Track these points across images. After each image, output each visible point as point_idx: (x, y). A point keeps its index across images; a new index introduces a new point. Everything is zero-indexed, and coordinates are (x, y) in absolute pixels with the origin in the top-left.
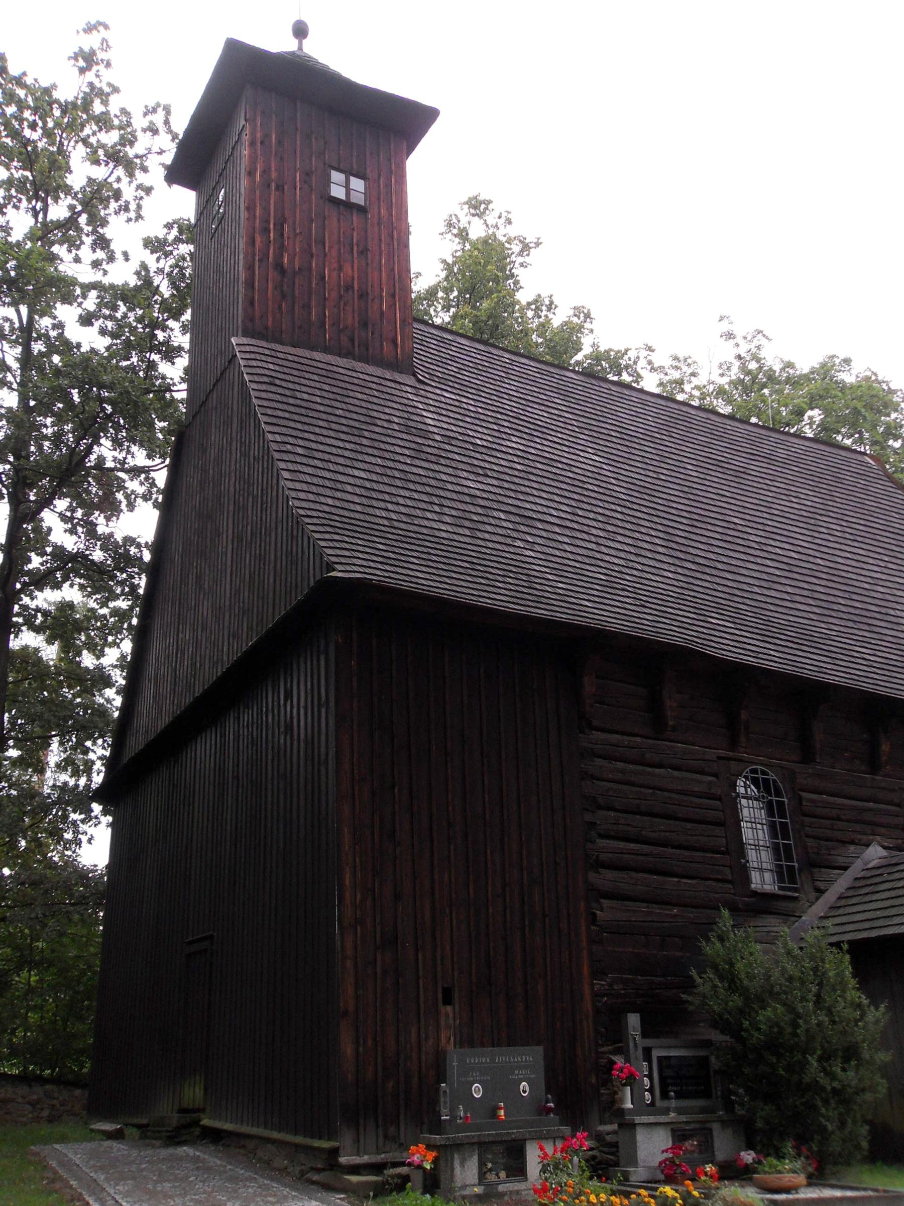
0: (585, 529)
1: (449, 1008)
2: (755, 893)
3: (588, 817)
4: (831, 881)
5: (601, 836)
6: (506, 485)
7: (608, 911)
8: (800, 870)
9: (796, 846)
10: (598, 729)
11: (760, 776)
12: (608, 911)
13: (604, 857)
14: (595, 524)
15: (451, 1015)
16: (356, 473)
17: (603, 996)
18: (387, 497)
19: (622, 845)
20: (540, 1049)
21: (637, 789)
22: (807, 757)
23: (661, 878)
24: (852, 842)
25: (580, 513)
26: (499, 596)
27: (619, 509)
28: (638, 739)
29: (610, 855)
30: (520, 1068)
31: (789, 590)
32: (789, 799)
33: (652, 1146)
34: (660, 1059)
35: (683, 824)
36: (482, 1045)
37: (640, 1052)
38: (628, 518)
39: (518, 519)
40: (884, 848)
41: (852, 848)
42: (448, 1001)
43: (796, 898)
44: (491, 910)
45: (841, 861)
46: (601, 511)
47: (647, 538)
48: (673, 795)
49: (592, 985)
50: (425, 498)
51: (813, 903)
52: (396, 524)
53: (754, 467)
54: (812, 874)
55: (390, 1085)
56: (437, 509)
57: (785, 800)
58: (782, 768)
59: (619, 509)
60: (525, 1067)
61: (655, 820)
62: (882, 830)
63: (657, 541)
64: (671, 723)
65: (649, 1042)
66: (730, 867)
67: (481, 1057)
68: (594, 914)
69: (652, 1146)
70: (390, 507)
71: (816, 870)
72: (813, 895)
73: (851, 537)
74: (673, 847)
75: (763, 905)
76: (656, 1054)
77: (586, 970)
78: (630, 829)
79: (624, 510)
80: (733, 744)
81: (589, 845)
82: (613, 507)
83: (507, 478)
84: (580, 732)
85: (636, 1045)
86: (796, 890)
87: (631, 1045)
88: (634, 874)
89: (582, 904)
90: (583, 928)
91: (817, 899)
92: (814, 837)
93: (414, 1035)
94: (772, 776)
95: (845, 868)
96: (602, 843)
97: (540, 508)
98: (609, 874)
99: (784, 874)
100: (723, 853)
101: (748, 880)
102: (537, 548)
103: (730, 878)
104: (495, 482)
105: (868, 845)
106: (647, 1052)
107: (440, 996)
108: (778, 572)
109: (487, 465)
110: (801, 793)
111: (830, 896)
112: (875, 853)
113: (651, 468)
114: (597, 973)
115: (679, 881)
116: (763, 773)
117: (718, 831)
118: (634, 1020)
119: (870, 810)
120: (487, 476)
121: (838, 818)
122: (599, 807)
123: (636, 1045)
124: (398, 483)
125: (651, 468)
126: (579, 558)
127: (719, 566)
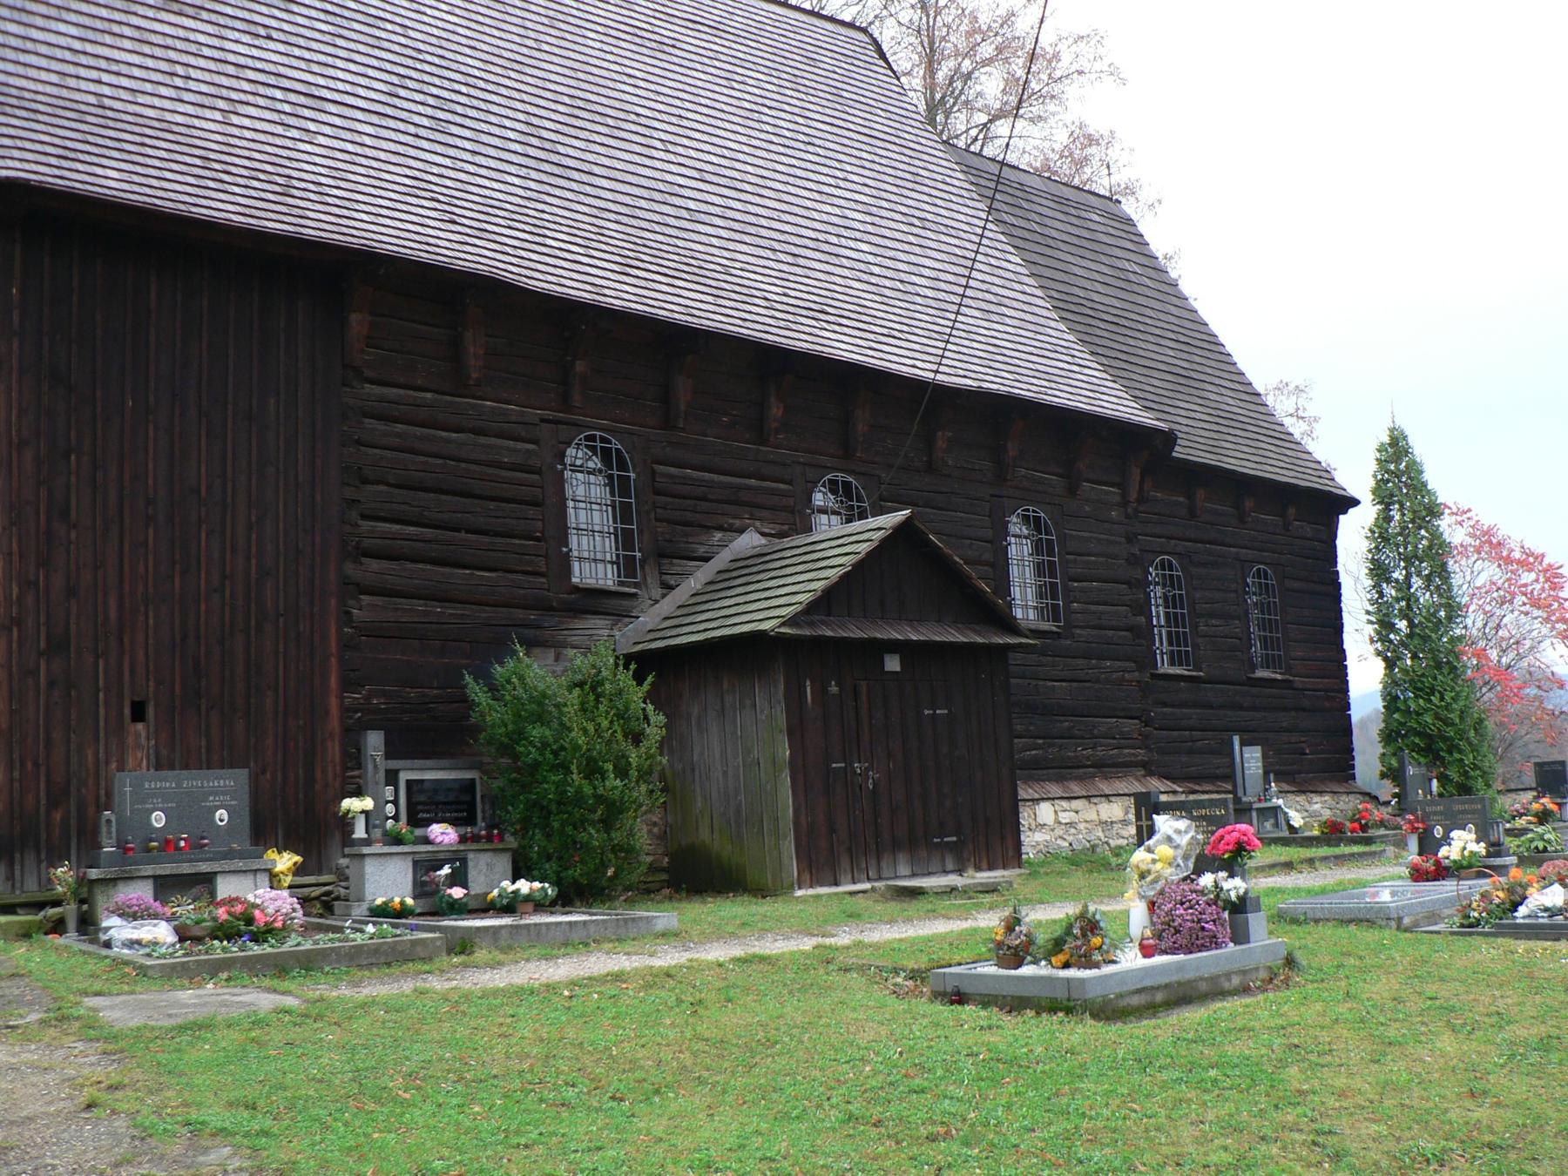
0: (404, 115)
1: (140, 726)
2: (576, 589)
3: (349, 493)
4: (686, 575)
5: (364, 517)
6: (297, 52)
7: (365, 610)
8: (643, 561)
9: (640, 532)
10: (372, 382)
11: (599, 444)
12: (365, 610)
13: (367, 543)
14: (421, 109)
15: (144, 735)
16: (62, 27)
17: (356, 711)
18: (103, 64)
19: (396, 527)
20: (242, 774)
21: (422, 459)
22: (667, 423)
23: (447, 570)
24: (720, 528)
25: (402, 92)
26: (226, 205)
27: (464, 89)
28: (429, 395)
29: (379, 541)
30: (216, 794)
31: (692, 204)
32: (638, 474)
33: (388, 880)
34: (408, 782)
35: (481, 502)
36: (172, 767)
37: (381, 775)
38: (476, 103)
39: (302, 100)
40: (763, 534)
41: (718, 535)
42: (138, 714)
43: (635, 595)
44: (203, 607)
45: (701, 550)
46: (435, 91)
47: (497, 131)
48: (473, 467)
49: (342, 698)
50: (164, 66)
51: (657, 602)
52: (107, 102)
53: (690, 40)
54: (660, 565)
55: (58, 816)
56: (179, 82)
57: (632, 475)
58: (632, 433)
59: (464, 89)
60: (224, 793)
61: (444, 497)
62: (765, 513)
63: (511, 135)
64: (475, 375)
65: (393, 764)
66: (546, 557)
67: (168, 782)
68: (348, 613)
69: (388, 880)
70: (105, 77)
71: (666, 561)
72: (657, 592)
73: (806, 139)
74: (467, 532)
75: (593, 601)
76: (404, 777)
77: (333, 681)
78: (407, 508)
79: (472, 92)
80: (565, 403)
81: (347, 528)
82: (456, 87)
83: (302, 42)
84: (344, 385)
85: (375, 766)
86: (636, 585)
87: (370, 767)
88: (410, 565)
89: (333, 602)
90: (333, 630)
91: (664, 596)
92: (669, 521)
93: (90, 758)
94: (616, 444)
95: (707, 560)
96: (366, 525)
97: (340, 86)
98: (375, 565)
99: (627, 567)
100: (538, 539)
101: (568, 571)
102: (321, 140)
103: (544, 569)
104: (281, 48)
105: (741, 531)
106: (392, 778)
107: (127, 711)
108: (681, 181)
109: (274, 23)
110: (656, 467)
111: (681, 594)
112: (749, 541)
113: (531, 34)
114: (348, 684)
115: (994, 593)
116: (603, 440)
117: (532, 512)
118: (374, 741)
119: (749, 488)
120: (269, 38)
121: (704, 499)
122: (366, 481)
123: (375, 766)
124: (128, 44)
125: (531, 34)
126: (382, 155)
127: (596, 170)
